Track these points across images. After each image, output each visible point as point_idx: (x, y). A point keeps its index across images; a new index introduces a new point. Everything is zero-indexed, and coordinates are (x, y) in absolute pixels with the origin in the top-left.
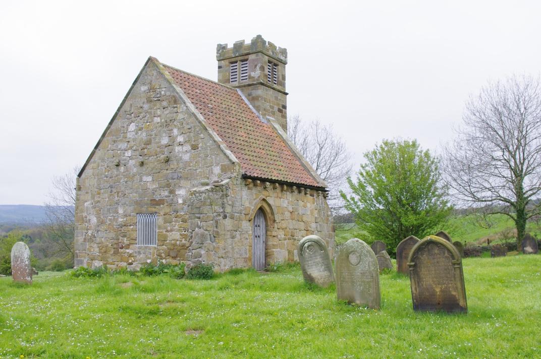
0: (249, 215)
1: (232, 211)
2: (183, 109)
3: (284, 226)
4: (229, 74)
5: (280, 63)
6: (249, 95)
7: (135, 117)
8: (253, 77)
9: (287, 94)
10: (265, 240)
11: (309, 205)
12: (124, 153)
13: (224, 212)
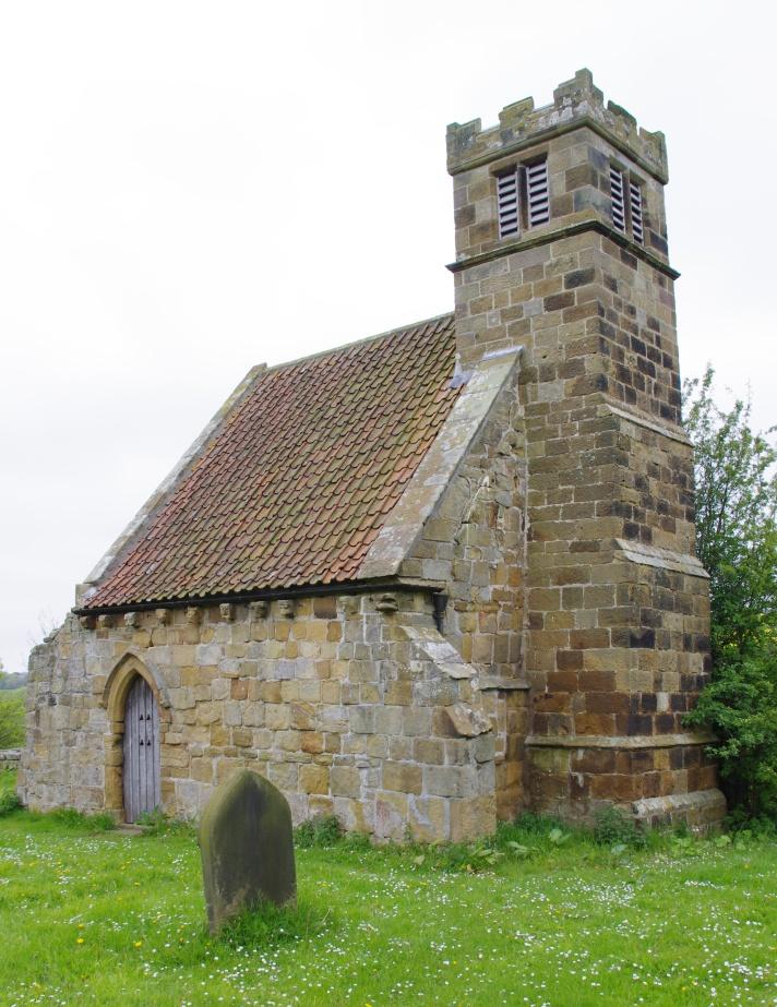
11: (308, 649)
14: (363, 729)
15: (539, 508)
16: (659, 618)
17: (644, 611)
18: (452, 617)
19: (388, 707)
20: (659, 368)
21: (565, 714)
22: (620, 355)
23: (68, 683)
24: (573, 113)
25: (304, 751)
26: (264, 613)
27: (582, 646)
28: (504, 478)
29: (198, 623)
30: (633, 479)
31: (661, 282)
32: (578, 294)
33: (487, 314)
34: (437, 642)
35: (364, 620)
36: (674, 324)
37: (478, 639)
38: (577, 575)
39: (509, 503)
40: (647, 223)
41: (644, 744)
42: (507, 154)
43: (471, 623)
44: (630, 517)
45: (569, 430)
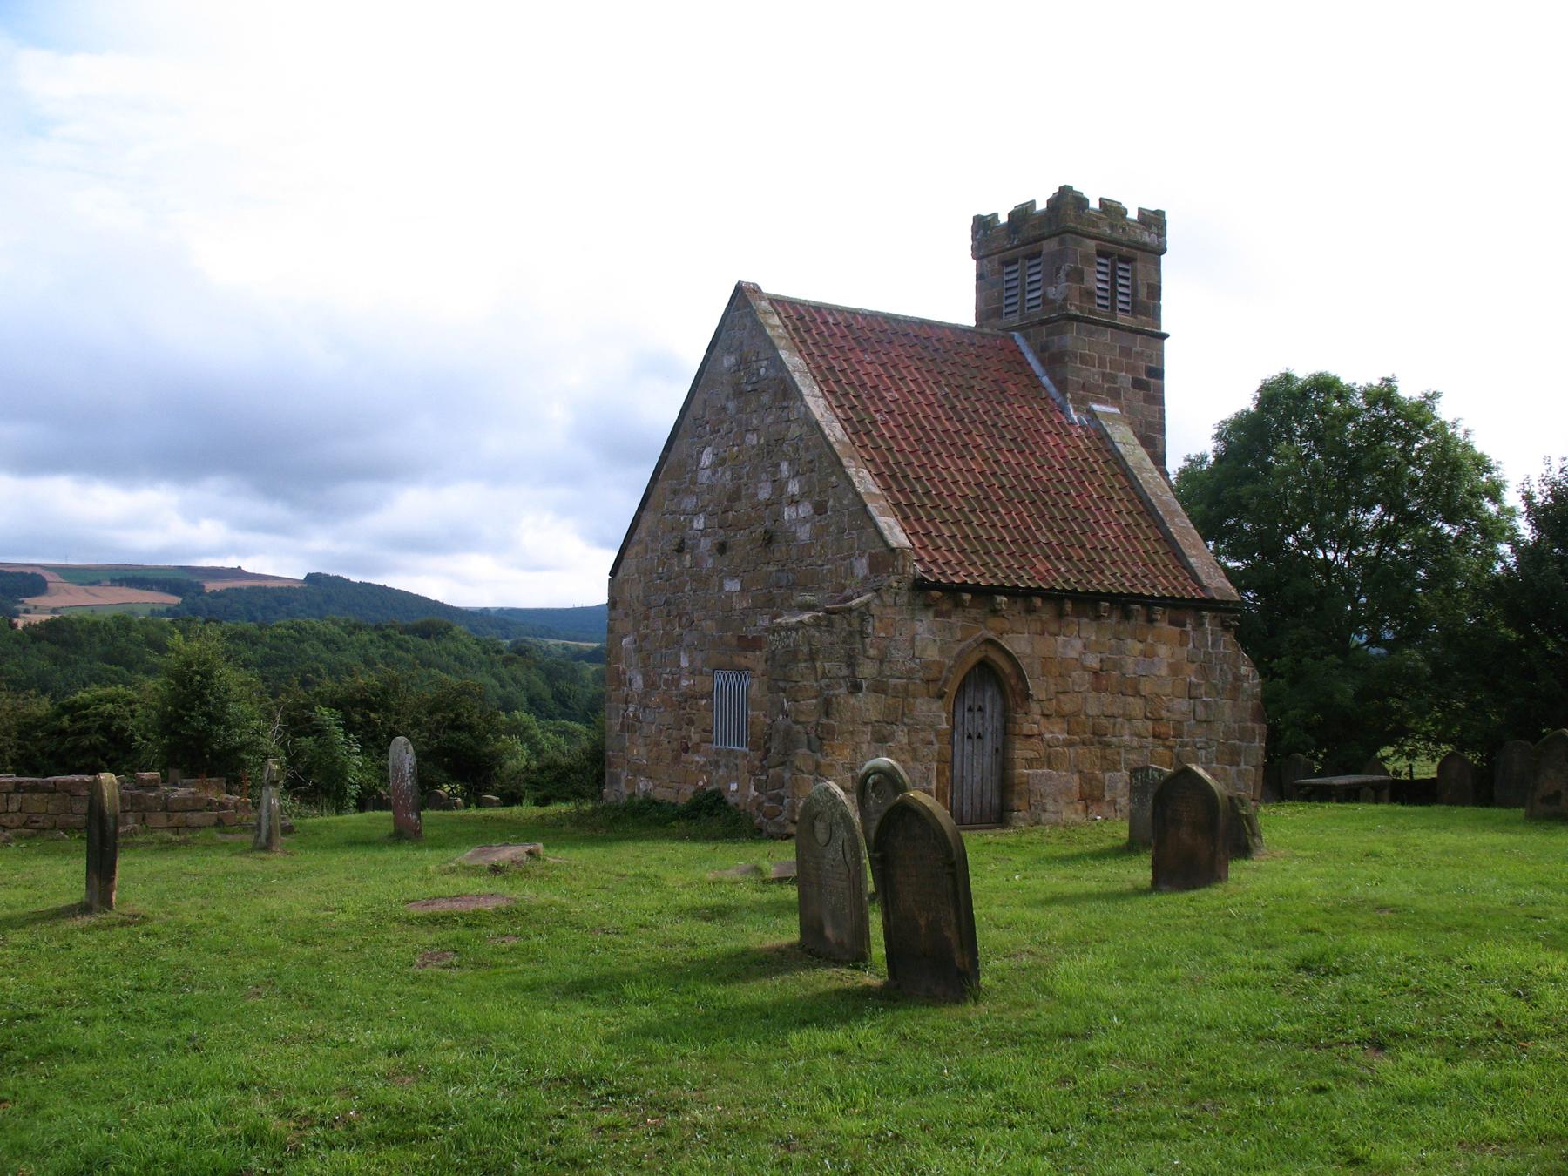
0: (941, 683)
1: (880, 673)
2: (799, 412)
3: (1068, 707)
4: (1000, 294)
5: (1139, 253)
6: (1044, 348)
7: (712, 434)
8: (1053, 301)
9: (1166, 336)
10: (999, 746)
11: (1163, 650)
12: (691, 521)
13: (854, 676)
21: (245, 757)
23: (886, 667)
33: (1092, 369)
35: (1209, 632)
36: (1164, 435)
42: (1110, 242)
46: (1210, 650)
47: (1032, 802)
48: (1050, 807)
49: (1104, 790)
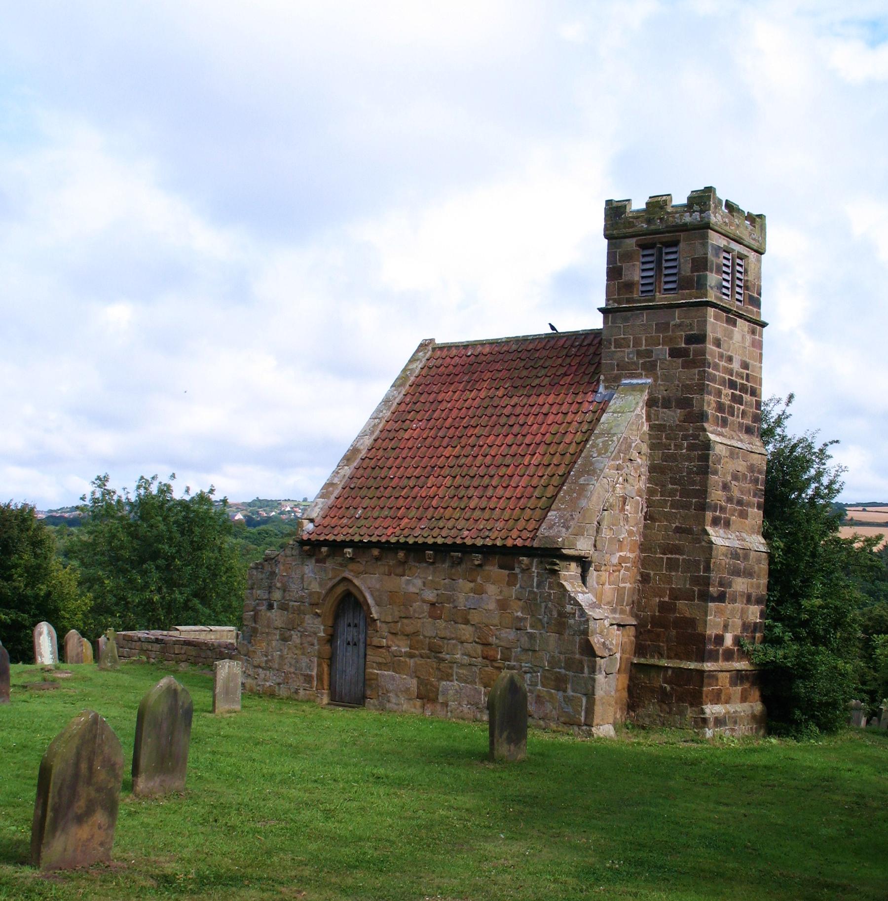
1: (283, 598)
14: (527, 646)
15: (654, 498)
16: (731, 582)
17: (720, 578)
18: (592, 574)
19: (548, 634)
20: (747, 397)
22: (719, 393)
23: (287, 594)
24: (701, 217)
25: (484, 658)
26: (460, 562)
27: (677, 598)
28: (631, 477)
29: (403, 563)
30: (721, 484)
31: (753, 332)
32: (693, 350)
33: (626, 350)
34: (583, 593)
35: (535, 574)
36: (761, 362)
37: (607, 590)
38: (677, 550)
39: (634, 495)
40: (746, 288)
41: (713, 668)
43: (603, 578)
44: (716, 512)
45: (678, 447)
46: (535, 590)
47: (380, 694)
48: (394, 700)
49: (438, 694)
